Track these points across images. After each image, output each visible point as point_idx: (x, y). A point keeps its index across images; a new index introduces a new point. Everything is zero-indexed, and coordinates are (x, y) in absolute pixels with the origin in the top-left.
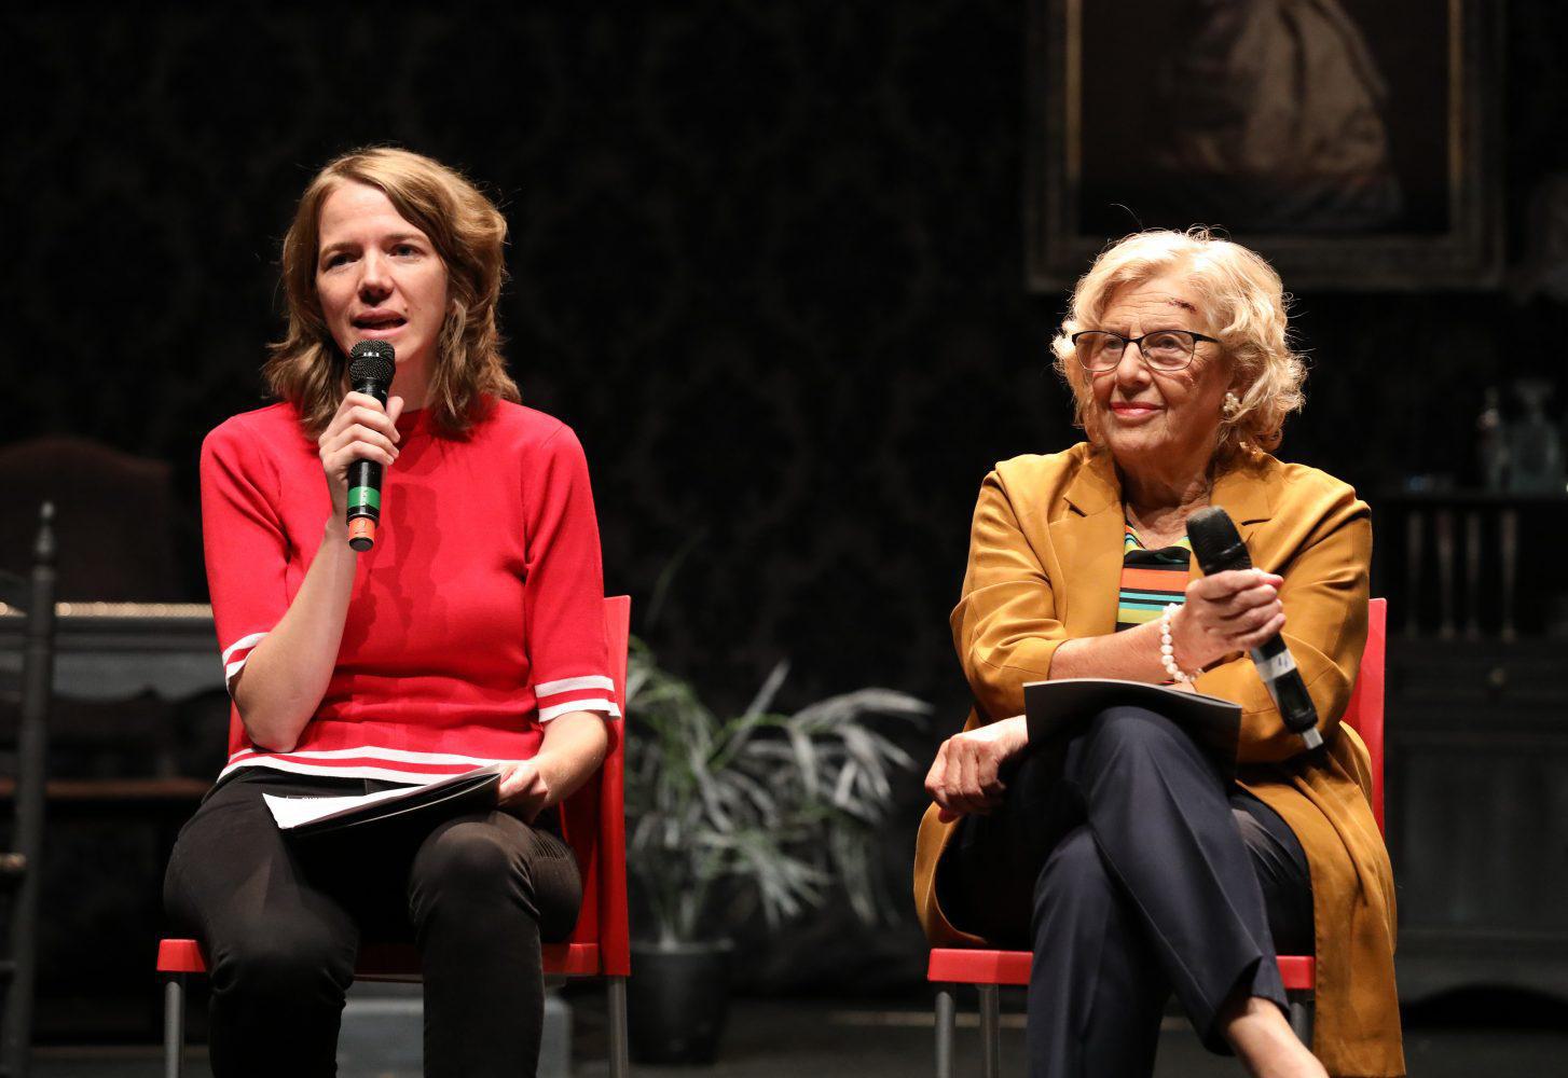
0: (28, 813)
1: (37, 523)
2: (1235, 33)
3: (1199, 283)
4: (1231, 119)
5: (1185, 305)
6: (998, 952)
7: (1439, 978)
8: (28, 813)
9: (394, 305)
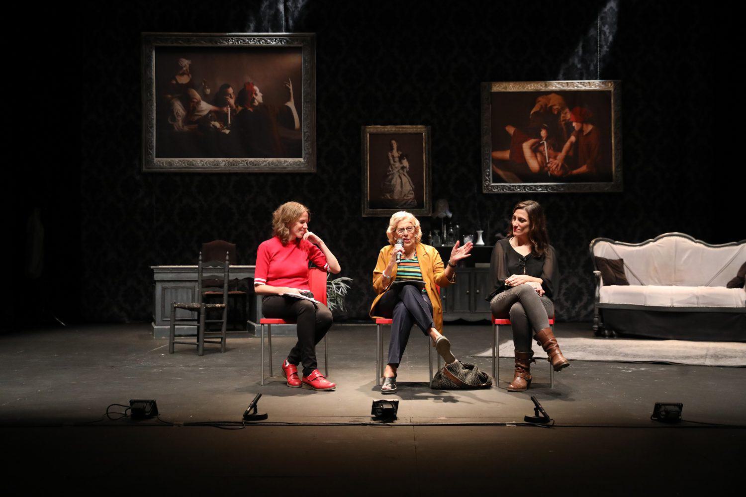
0: (225, 297)
1: (199, 255)
2: (392, 179)
4: (392, 191)
6: (278, 319)
7: (450, 318)
8: (225, 297)
9: (408, 238)
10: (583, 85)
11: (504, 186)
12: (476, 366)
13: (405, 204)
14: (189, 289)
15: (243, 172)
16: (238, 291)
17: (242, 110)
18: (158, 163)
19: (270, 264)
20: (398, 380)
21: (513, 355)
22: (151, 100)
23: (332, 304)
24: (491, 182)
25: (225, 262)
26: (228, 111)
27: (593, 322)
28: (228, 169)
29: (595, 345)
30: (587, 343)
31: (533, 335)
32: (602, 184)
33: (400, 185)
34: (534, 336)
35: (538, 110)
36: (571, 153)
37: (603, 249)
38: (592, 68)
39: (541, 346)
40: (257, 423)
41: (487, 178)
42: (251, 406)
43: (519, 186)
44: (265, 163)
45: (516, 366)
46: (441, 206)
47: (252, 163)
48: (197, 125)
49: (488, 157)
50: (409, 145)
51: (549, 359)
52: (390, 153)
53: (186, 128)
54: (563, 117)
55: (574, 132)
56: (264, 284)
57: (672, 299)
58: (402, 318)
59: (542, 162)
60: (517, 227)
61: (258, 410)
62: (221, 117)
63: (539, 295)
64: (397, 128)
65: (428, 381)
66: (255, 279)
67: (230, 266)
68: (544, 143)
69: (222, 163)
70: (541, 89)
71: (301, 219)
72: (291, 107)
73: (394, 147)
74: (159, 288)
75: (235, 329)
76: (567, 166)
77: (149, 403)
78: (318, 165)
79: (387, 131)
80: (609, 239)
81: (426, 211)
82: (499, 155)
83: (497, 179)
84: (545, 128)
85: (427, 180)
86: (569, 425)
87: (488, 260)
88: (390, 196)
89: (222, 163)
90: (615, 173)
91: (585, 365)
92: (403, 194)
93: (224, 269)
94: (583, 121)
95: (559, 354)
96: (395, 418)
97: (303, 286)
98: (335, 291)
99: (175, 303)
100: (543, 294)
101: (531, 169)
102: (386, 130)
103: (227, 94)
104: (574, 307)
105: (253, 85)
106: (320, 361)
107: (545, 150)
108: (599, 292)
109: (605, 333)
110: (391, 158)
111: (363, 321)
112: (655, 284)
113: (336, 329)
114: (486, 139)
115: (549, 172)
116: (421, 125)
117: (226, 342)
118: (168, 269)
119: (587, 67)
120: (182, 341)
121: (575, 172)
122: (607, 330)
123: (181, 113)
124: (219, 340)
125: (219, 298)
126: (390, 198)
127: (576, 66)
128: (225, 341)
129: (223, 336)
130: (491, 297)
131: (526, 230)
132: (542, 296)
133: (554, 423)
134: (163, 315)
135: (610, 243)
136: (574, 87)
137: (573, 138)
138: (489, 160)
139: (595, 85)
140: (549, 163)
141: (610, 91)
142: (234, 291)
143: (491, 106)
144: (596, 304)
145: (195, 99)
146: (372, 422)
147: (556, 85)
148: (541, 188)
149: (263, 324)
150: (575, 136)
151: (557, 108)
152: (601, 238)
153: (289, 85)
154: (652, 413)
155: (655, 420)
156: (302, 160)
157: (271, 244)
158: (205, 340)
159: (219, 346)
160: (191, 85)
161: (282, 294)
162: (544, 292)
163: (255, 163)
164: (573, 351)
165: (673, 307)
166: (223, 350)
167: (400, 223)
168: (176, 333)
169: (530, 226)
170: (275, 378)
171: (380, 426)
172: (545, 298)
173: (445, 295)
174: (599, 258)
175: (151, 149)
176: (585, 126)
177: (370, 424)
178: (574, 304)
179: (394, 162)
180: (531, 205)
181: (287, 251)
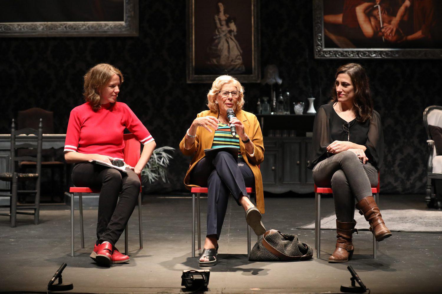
0: (39, 167)
2: (219, 43)
4: (218, 56)
8: (39, 167)
11: (337, 51)
12: (296, 236)
13: (232, 69)
15: (62, 36)
16: (55, 161)
20: (220, 252)
21: (335, 227)
23: (154, 175)
24: (323, 47)
27: (425, 194)
30: (418, 215)
31: (355, 204)
32: (438, 50)
33: (227, 49)
36: (406, 18)
42: (55, 276)
43: (353, 52)
45: (338, 237)
46: (271, 72)
47: (71, 27)
49: (319, 21)
52: (216, 16)
56: (75, 151)
58: (216, 187)
59: (376, 27)
60: (341, 92)
61: (63, 280)
63: (363, 163)
65: (246, 253)
66: (66, 146)
67: (43, 135)
71: (112, 83)
76: (401, 32)
83: (329, 43)
85: (256, 45)
88: (217, 62)
89: (40, 27)
91: (412, 236)
92: (230, 59)
95: (381, 224)
97: (114, 155)
98: (157, 161)
100: (366, 162)
101: (365, 34)
104: (408, 179)
107: (378, 15)
109: (437, 205)
110: (218, 21)
111: (188, 194)
115: (383, 37)
117: (40, 214)
121: (410, 37)
125: (32, 168)
126: (216, 63)
130: (314, 165)
131: (351, 95)
132: (366, 163)
140: (383, 27)
142: (51, 161)
148: (375, 54)
152: (435, 106)
156: (123, 23)
157: (81, 111)
158: (18, 211)
159: (32, 217)
161: (91, 161)
162: (367, 159)
163: (74, 27)
169: (354, 89)
172: (369, 166)
178: (409, 175)
179: (221, 25)
181: (99, 117)
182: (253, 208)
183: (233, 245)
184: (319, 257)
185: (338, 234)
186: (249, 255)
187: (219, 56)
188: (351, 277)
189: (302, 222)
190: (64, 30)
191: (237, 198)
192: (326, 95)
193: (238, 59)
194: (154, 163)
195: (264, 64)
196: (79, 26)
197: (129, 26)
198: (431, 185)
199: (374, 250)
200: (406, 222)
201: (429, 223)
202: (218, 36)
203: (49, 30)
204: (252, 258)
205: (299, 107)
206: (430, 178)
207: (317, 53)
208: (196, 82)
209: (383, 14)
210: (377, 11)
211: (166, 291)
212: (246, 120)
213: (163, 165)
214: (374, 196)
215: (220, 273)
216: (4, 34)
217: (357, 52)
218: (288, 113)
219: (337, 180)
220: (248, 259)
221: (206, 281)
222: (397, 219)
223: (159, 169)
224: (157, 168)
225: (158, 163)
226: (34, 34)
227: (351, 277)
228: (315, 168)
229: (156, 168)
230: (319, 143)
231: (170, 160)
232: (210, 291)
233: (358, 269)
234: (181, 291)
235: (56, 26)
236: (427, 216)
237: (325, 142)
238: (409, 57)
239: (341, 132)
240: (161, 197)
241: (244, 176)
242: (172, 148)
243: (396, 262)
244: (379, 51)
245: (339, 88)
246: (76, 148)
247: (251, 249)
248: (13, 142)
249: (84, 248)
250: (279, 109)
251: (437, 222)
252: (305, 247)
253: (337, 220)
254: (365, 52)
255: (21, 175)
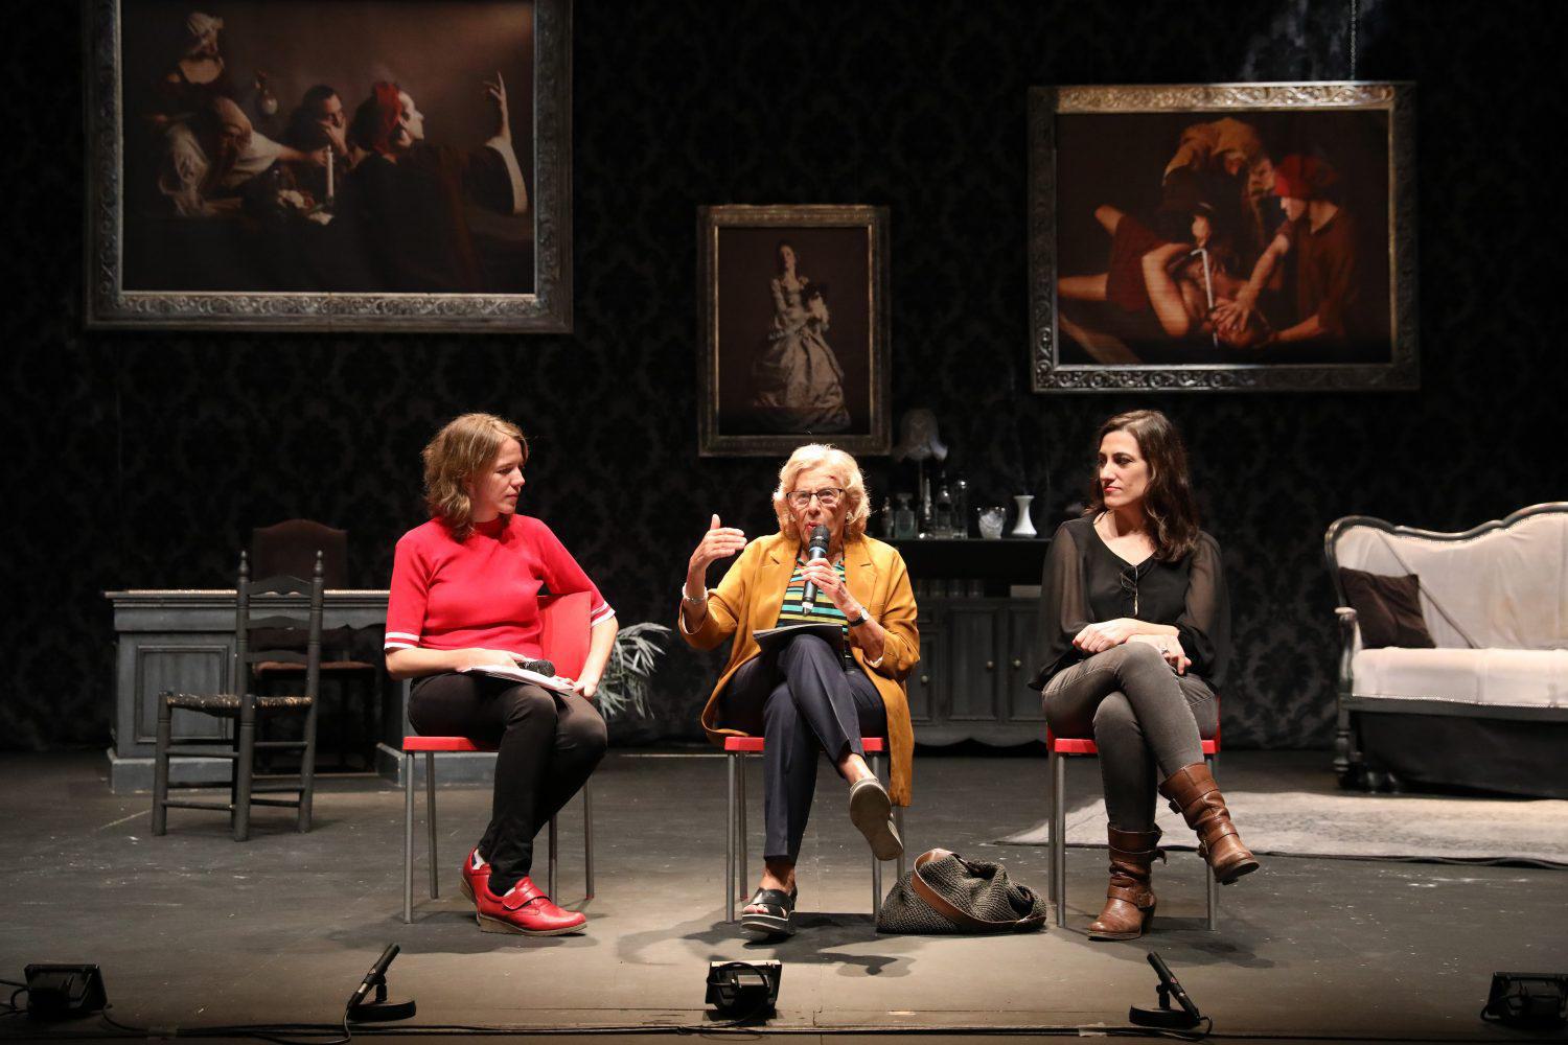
0: (312, 678)
2: (782, 351)
3: (834, 468)
5: (832, 477)
7: (940, 736)
8: (312, 678)
10: (1311, 94)
11: (1092, 372)
12: (1001, 868)
13: (818, 421)
14: (212, 656)
15: (371, 330)
16: (352, 659)
17: (367, 160)
18: (131, 304)
19: (427, 591)
21: (1104, 839)
22: (110, 128)
23: (613, 696)
24: (1056, 362)
25: (311, 580)
26: (326, 162)
28: (325, 322)
29: (1339, 813)
32: (1362, 368)
34: (1160, 786)
35: (1186, 163)
36: (1276, 284)
37: (1360, 547)
38: (1335, 47)
39: (1181, 814)
40: (393, 1027)
41: (1045, 351)
43: (1134, 374)
44: (430, 305)
45: (1112, 870)
46: (918, 427)
48: (239, 200)
49: (1046, 294)
50: (828, 258)
51: (1202, 851)
52: (776, 282)
53: (209, 208)
54: (1255, 183)
55: (1284, 224)
57: (1552, 687)
59: (1196, 308)
60: (1112, 481)
62: (306, 176)
64: (796, 210)
65: (869, 911)
67: (326, 592)
68: (1200, 254)
69: (311, 304)
70: (1193, 106)
71: (501, 462)
72: (504, 156)
73: (788, 265)
74: (127, 651)
75: (343, 768)
76: (1263, 319)
77: (80, 975)
78: (579, 313)
79: (771, 219)
80: (1377, 520)
81: (876, 438)
82: (1076, 286)
83: (1071, 352)
84: (1204, 214)
86: (1252, 1034)
87: (1035, 579)
88: (777, 400)
89: (310, 306)
90: (1399, 335)
91: (1307, 867)
92: (813, 393)
93: (304, 601)
94: (1310, 194)
95: (1230, 838)
96: (772, 1013)
98: (623, 662)
99: (170, 694)
100: (1188, 669)
101: (1166, 326)
102: (766, 216)
103: (326, 114)
104: (1283, 710)
105: (398, 89)
106: (539, 861)
107: (1203, 276)
108: (1349, 665)
109: (1367, 780)
110: (779, 295)
111: (702, 745)
112: (1508, 644)
113: (627, 766)
114: (1042, 243)
115: (1215, 335)
116: (861, 202)
117: (314, 803)
118: (153, 599)
119: (1321, 47)
120: (188, 800)
121: (1287, 334)
122: (1373, 769)
123: (196, 165)
124: (295, 797)
125: (292, 680)
126: (775, 405)
127: (1292, 43)
128: (311, 797)
129: (303, 786)
130: (1044, 679)
133: (1210, 1029)
134: (139, 729)
135: (1382, 532)
136: (1284, 101)
137: (1281, 242)
138: (1050, 301)
139: (1342, 94)
140: (1214, 309)
141: (1385, 113)
142: (341, 660)
143: (1055, 151)
144: (1342, 699)
145: (236, 126)
146: (708, 1023)
147: (1235, 96)
149: (411, 752)
150: (1286, 235)
151: (1238, 159)
152: (1356, 518)
153: (499, 92)
154: (1484, 1001)
155: (1495, 1021)
156: (532, 298)
159: (292, 813)
160: (223, 87)
162: (1189, 661)
163: (402, 306)
164: (1277, 829)
165: (1557, 709)
166: (304, 824)
167: (802, 475)
168: (174, 778)
170: (444, 902)
171: (731, 1036)
172: (1193, 681)
173: (925, 674)
174: (1352, 571)
175: (109, 266)
176: (1314, 208)
177: (701, 1031)
178: (1283, 698)
179: (789, 305)
180: (1142, 421)
182: (870, 780)
183: (834, 887)
184: (1061, 923)
185: (1114, 864)
186: (877, 919)
187: (784, 387)
188: (1160, 982)
189: (1006, 825)
190: (374, 313)
191: (835, 757)
192: (1072, 487)
193: (832, 394)
194: (614, 667)
195: (900, 406)
196: (415, 303)
197: (549, 305)
198: (1348, 727)
199: (1209, 906)
200: (1286, 826)
201: (1348, 831)
202: (782, 334)
203: (336, 313)
204: (883, 926)
205: (992, 520)
206: (1345, 709)
207: (1039, 377)
208: (722, 454)
209: (1216, 273)
210: (1199, 265)
211: (666, 1018)
212: (868, 562)
213: (638, 670)
214: (1209, 761)
215: (804, 966)
216: (213, 323)
217: (1144, 375)
218: (963, 535)
219: (1111, 720)
220: (875, 928)
221: (771, 992)
222: (1260, 820)
223: (627, 682)
224: (623, 681)
225: (625, 667)
226: (292, 323)
227: (1160, 982)
228: (1050, 687)
229: (619, 678)
230: (1060, 622)
231: (657, 657)
232: (782, 1017)
233: (1173, 958)
234: (704, 1019)
235: (355, 302)
236: (1341, 811)
237: (1075, 620)
238: (1282, 387)
239: (1117, 590)
240: (631, 756)
241: (858, 703)
242: (662, 628)
243: (1273, 939)
244: (1203, 371)
245: (1108, 470)
246: (416, 638)
247: (883, 902)
248: (243, 611)
249: (437, 897)
250: (940, 524)
251: (1369, 827)
252: (1025, 896)
253: (1109, 824)
254: (1166, 374)
255: (264, 701)
